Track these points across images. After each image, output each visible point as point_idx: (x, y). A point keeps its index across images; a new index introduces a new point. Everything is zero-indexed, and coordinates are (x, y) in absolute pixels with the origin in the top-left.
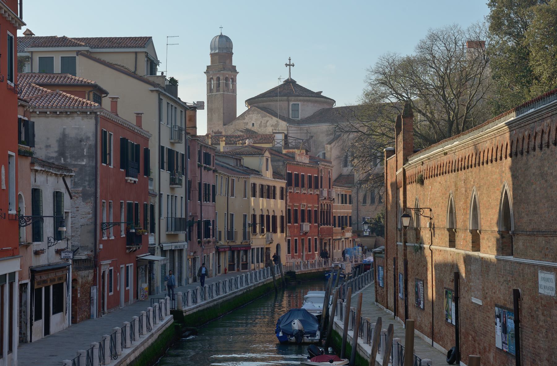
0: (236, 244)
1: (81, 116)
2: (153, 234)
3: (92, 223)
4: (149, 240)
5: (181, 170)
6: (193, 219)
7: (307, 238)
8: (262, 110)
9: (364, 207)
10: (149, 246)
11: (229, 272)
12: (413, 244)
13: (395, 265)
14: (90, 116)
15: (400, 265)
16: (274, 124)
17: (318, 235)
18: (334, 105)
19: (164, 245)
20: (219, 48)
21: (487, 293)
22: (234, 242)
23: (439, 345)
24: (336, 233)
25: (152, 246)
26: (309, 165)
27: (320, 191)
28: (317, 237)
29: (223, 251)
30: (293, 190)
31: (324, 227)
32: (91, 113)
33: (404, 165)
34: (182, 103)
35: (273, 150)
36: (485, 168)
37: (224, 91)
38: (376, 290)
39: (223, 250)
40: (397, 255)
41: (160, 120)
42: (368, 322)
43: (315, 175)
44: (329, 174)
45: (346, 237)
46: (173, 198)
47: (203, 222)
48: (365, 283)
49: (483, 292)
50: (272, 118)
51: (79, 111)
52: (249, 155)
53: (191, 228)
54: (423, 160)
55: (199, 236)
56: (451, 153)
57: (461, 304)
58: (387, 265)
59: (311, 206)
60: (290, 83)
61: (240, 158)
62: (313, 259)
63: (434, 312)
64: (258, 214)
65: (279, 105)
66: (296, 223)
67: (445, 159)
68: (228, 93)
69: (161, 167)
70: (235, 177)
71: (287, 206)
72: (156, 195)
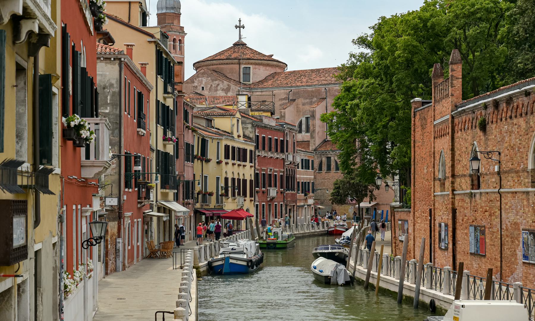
0: (210, 207)
1: (105, 62)
3: (115, 173)
7: (274, 203)
9: (319, 174)
14: (115, 62)
16: (225, 88)
18: (286, 69)
22: (208, 205)
24: (299, 200)
28: (282, 203)
32: (114, 59)
43: (281, 139)
44: (294, 138)
51: (102, 57)
60: (240, 45)
64: (230, 177)
65: (230, 69)
66: (264, 187)
69: (157, 122)
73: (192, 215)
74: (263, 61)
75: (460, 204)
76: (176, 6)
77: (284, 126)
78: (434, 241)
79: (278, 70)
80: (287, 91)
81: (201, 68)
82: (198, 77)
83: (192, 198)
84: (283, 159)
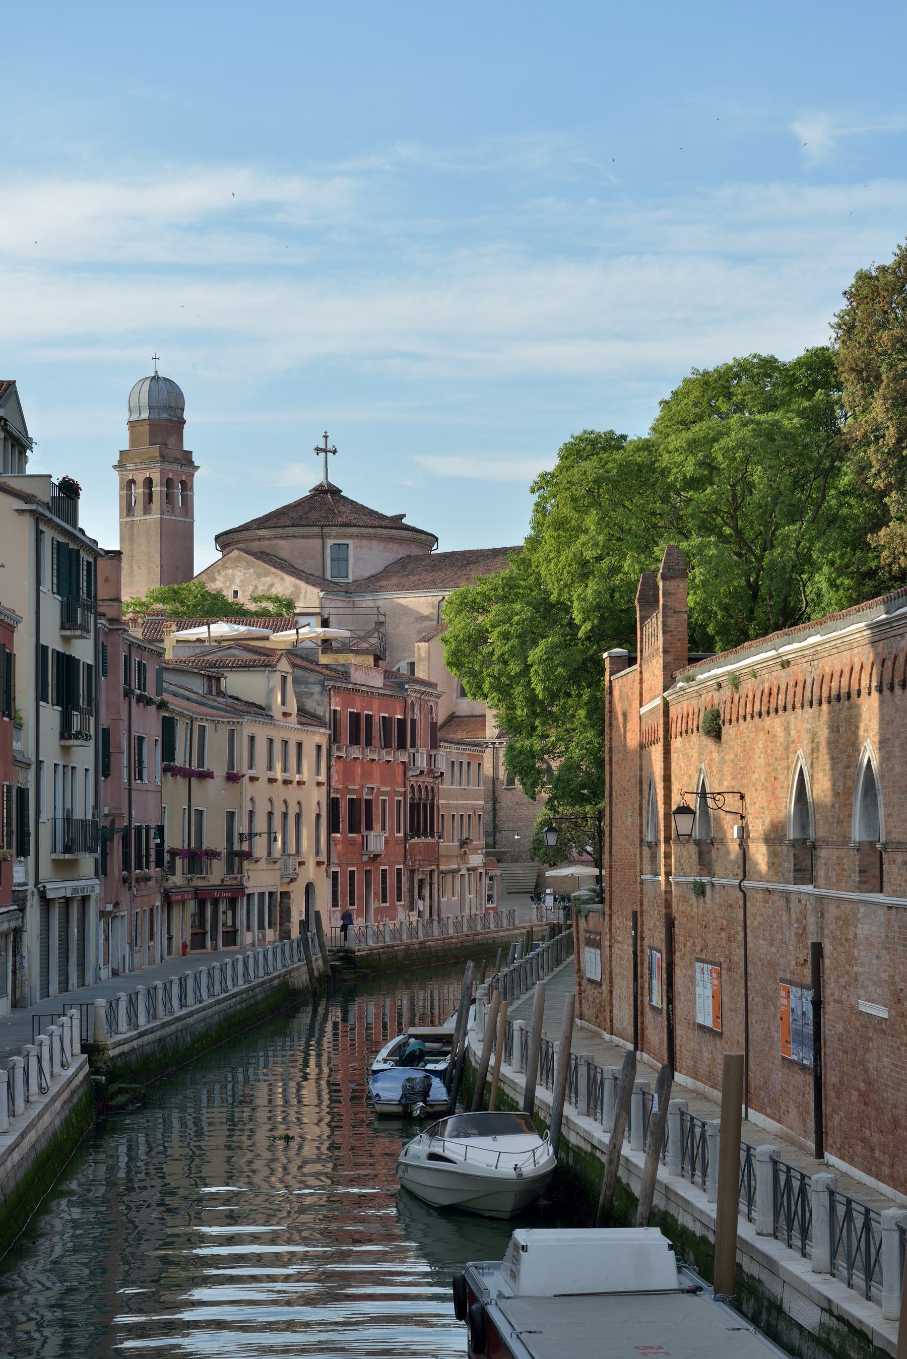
0: (211, 883)
2: (22, 859)
4: (15, 875)
5: (85, 703)
6: (113, 822)
7: (377, 868)
8: (258, 558)
9: (509, 793)
10: (14, 888)
11: (192, 952)
12: (691, 879)
13: (635, 928)
15: (649, 929)
17: (405, 862)
18: (435, 547)
19: (48, 886)
20: (150, 408)
21: (902, 990)
23: (764, 1117)
24: (446, 857)
25: (20, 889)
26: (384, 692)
27: (409, 754)
28: (401, 866)
29: (178, 902)
30: (346, 752)
31: (419, 840)
33: (665, 690)
34: (87, 541)
35: (296, 656)
36: (897, 699)
37: (162, 513)
38: (580, 989)
39: (179, 898)
40: (642, 904)
41: (38, 583)
42: (589, 1064)
44: (431, 713)
45: (470, 865)
46: (68, 770)
47: (133, 831)
48: (538, 976)
49: (892, 988)
50: (282, 579)
52: (240, 667)
53: (108, 843)
54: (720, 679)
55: (126, 866)
56: (799, 661)
57: (827, 1016)
58: (610, 930)
59: (387, 792)
61: (217, 675)
62: (393, 918)
63: (750, 1037)
67: (783, 677)
68: (173, 518)
69: (41, 695)
70: (207, 720)
71: (332, 791)
72: (29, 765)
73: (158, 904)
74: (379, 531)
75: (681, 909)
76: (173, 404)
77: (406, 686)
78: (642, 988)
79: (416, 551)
80: (434, 598)
81: (232, 547)
82: (224, 567)
83: (158, 865)
84: (403, 763)
